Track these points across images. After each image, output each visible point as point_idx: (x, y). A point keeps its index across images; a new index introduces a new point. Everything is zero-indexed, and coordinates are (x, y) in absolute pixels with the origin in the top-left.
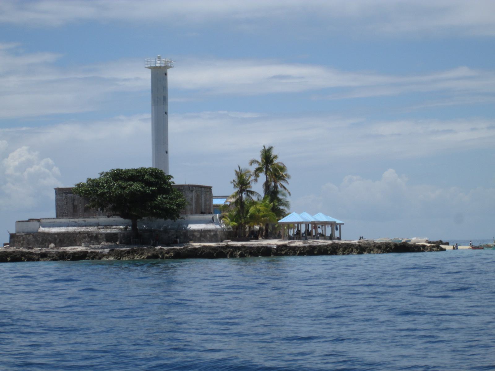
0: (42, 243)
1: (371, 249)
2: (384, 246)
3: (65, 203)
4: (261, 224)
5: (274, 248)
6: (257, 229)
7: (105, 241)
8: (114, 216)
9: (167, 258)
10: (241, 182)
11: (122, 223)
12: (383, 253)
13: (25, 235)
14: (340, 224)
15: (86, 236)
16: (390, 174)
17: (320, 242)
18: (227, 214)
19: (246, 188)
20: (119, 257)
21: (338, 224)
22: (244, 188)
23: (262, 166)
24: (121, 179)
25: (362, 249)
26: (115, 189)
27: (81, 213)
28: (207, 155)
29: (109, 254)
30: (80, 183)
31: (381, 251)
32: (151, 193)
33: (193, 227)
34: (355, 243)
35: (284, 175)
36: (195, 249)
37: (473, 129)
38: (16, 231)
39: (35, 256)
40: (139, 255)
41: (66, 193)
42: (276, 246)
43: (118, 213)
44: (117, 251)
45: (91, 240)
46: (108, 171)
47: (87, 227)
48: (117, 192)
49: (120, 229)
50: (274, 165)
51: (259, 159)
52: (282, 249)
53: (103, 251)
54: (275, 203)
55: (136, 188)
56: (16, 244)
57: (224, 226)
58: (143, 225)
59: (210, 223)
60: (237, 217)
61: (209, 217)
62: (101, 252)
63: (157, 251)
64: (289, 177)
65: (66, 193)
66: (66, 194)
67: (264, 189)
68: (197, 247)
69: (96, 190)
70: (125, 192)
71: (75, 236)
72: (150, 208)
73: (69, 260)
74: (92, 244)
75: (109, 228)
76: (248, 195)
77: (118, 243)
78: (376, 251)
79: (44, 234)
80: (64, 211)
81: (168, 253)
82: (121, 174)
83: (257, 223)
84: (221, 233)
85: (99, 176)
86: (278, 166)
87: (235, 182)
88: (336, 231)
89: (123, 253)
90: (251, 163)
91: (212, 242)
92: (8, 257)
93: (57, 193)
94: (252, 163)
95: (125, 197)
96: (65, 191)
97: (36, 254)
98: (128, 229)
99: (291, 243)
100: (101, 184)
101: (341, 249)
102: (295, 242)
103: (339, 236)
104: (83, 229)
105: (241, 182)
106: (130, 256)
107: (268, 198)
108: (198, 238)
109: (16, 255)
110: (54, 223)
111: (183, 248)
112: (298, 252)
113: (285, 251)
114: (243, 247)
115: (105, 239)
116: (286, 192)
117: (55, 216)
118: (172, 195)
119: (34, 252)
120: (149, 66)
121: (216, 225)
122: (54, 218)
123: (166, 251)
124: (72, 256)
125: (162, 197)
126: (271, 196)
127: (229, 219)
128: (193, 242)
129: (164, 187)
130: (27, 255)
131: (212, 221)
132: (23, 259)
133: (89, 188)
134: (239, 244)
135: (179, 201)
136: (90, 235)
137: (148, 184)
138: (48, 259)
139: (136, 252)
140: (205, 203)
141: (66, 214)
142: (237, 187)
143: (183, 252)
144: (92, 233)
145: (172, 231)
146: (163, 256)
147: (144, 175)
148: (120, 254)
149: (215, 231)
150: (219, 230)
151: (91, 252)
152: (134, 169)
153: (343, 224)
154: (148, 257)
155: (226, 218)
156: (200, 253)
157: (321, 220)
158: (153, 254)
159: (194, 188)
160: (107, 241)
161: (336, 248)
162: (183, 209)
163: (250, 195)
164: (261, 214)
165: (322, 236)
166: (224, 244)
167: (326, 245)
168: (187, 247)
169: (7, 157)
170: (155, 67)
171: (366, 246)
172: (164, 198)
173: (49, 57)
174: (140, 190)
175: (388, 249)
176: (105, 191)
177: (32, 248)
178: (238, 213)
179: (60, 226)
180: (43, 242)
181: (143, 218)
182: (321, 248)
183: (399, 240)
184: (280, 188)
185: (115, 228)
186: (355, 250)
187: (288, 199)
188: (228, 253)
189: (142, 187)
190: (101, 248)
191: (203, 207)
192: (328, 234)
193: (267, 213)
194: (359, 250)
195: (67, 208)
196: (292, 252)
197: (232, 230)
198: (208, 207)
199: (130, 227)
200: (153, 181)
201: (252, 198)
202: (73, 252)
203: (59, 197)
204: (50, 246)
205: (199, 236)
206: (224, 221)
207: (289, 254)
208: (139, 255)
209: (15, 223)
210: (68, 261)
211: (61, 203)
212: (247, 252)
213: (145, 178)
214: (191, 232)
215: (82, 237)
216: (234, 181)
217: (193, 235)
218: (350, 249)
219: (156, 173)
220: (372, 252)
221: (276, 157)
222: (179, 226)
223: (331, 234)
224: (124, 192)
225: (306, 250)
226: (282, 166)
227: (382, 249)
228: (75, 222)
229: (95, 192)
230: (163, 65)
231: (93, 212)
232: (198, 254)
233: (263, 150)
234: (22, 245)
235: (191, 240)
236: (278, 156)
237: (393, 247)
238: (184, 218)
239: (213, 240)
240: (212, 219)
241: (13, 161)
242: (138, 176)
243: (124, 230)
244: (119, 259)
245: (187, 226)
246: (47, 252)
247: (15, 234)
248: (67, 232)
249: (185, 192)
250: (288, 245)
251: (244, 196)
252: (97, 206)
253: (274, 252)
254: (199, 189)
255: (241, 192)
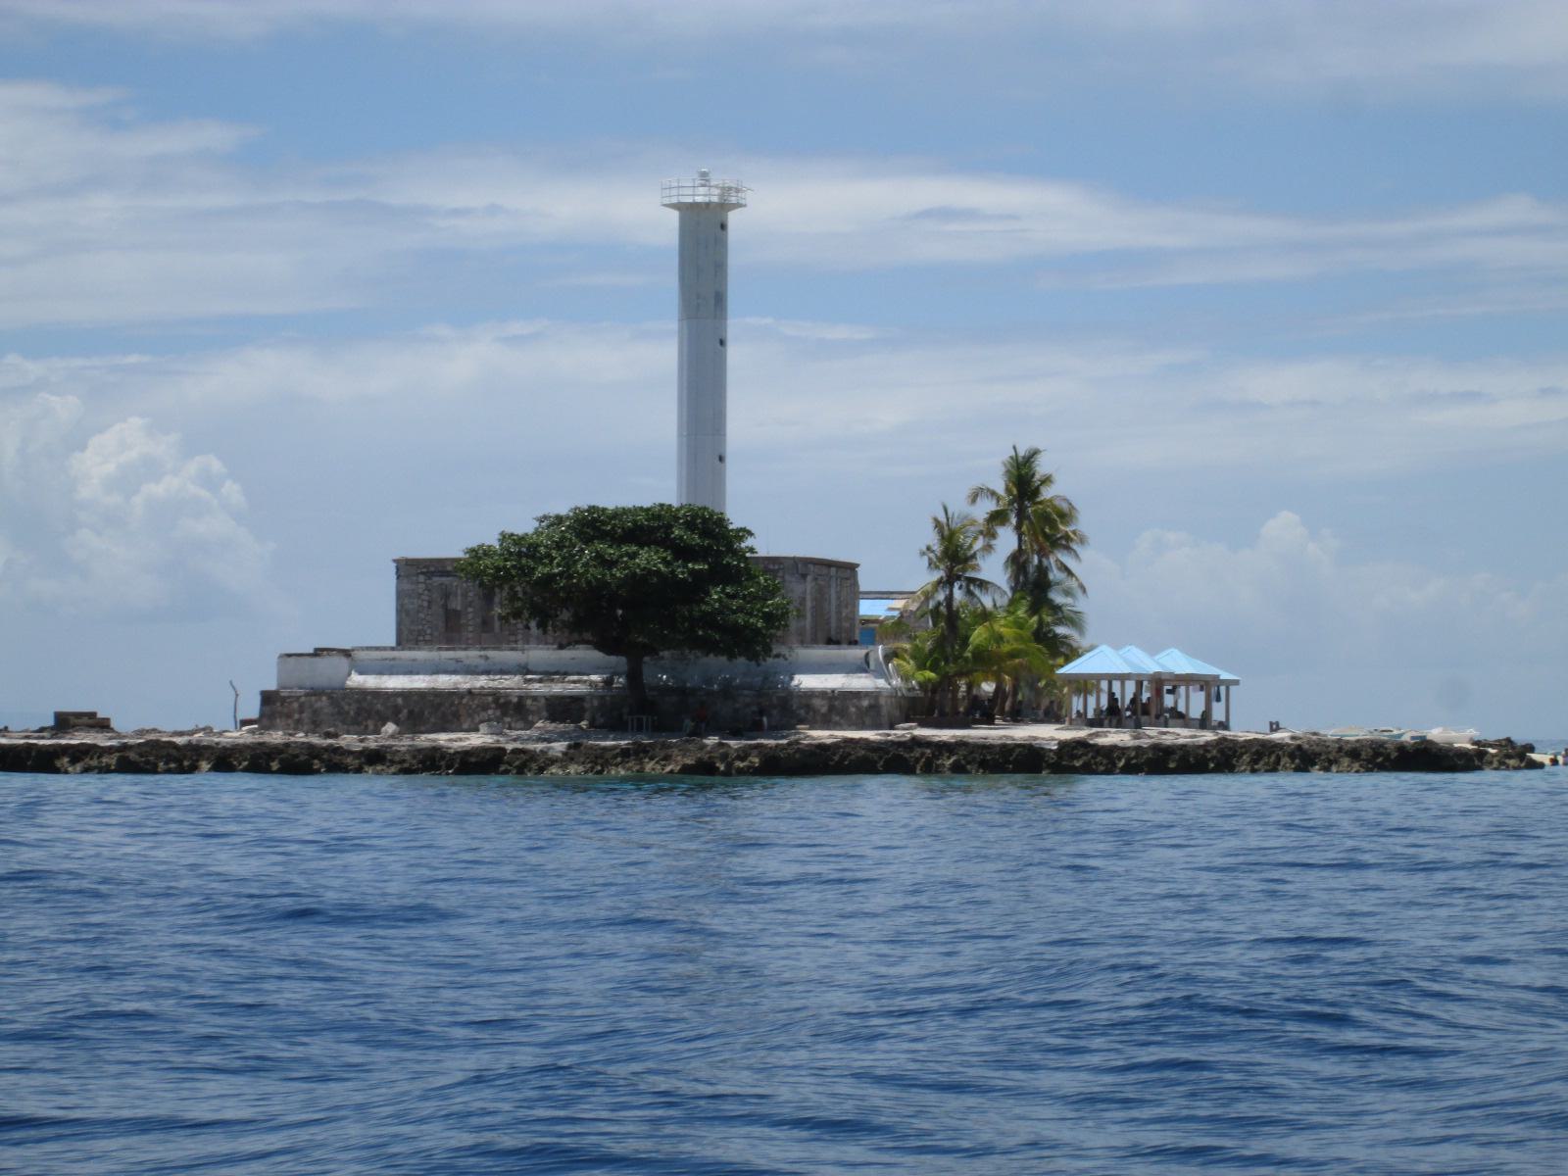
0: (356, 722)
1: (1332, 758)
2: (1369, 750)
3: (425, 604)
4: (1007, 677)
5: (1051, 750)
6: (989, 693)
7: (546, 719)
8: (577, 646)
9: (741, 772)
10: (950, 553)
11: (599, 668)
12: (1369, 770)
13: (307, 695)
14: (1229, 683)
15: (488, 703)
16: (1283, 527)
17: (1179, 735)
18: (907, 646)
19: (964, 570)
20: (599, 768)
21: (1224, 682)
22: (958, 570)
23: (1006, 507)
24: (603, 536)
25: (1307, 757)
26: (584, 565)
27: (470, 635)
28: (844, 469)
29: (568, 758)
30: (481, 546)
31: (1361, 766)
32: (690, 580)
33: (807, 682)
34: (1283, 739)
35: (1070, 534)
36: (822, 747)
37: (1546, 392)
38: (278, 684)
39: (349, 760)
40: (657, 763)
41: (429, 575)
42: (1056, 742)
43: (588, 636)
44: (592, 747)
45: (505, 714)
46: (563, 510)
47: (492, 677)
48: (592, 575)
49: (592, 684)
50: (1041, 503)
51: (1000, 487)
52: (1075, 752)
53: (549, 748)
54: (1044, 616)
55: (648, 563)
56: (278, 720)
57: (896, 682)
58: (660, 675)
59: (861, 672)
60: (936, 655)
61: (857, 653)
62: (541, 751)
63: (710, 752)
64: (1082, 541)
65: (429, 575)
66: (430, 578)
67: (1008, 575)
68: (829, 741)
69: (529, 567)
70: (614, 575)
71: (456, 702)
72: (686, 625)
73: (450, 772)
74: (507, 726)
75: (558, 681)
76: (969, 593)
77: (584, 724)
78: (1346, 764)
79: (363, 693)
80: (420, 627)
81: (742, 759)
82: (604, 523)
83: (990, 671)
84: (889, 701)
85: (537, 524)
86: (1054, 507)
87: (933, 551)
88: (1215, 705)
89: (608, 755)
90: (974, 498)
91: (861, 726)
92: (273, 761)
93: (402, 574)
94: (977, 495)
95: (615, 589)
96: (424, 567)
97: (351, 753)
98: (614, 686)
99: (1097, 735)
100: (542, 550)
101: (1244, 757)
102: (1109, 732)
103: (1224, 720)
104: (481, 682)
105: (950, 553)
106: (630, 764)
107: (1024, 601)
108: (824, 715)
109: (297, 756)
110: (392, 662)
111: (789, 744)
112: (1121, 764)
113: (1085, 758)
114: (961, 744)
115: (545, 714)
116: (1073, 583)
117: (392, 642)
118: (752, 587)
119: (345, 748)
120: (674, 200)
121: (876, 677)
122: (393, 649)
123: (737, 750)
124: (458, 760)
125: (723, 591)
126: (1031, 593)
127: (912, 662)
128: (807, 726)
129: (729, 564)
130: (325, 756)
131: (864, 667)
132: (315, 767)
133: (506, 560)
134: (946, 735)
135: (772, 604)
136: (502, 701)
137: (684, 552)
138: (388, 767)
139: (648, 752)
140: (839, 613)
141: (428, 638)
142: (937, 567)
143: (789, 754)
144: (507, 695)
145: (746, 692)
146: (729, 766)
147: (669, 527)
148: (602, 757)
149: (874, 695)
150: (885, 694)
151: (515, 751)
152: (641, 508)
153: (1236, 683)
154: (686, 770)
155: (905, 660)
156: (836, 758)
157: (1179, 671)
158: (700, 761)
159: (811, 567)
160: (553, 719)
161: (1230, 753)
162: (782, 628)
163: (977, 592)
164: (1006, 648)
165: (1180, 717)
166: (903, 736)
167: (1202, 743)
168: (797, 742)
169: (83, 447)
170: (691, 204)
171: (1317, 749)
172: (728, 595)
173: (216, 135)
174: (659, 569)
175: (1380, 760)
176: (556, 571)
177: (335, 736)
178: (940, 643)
179: (410, 670)
180: (360, 719)
181: (661, 654)
182: (1188, 751)
183: (1391, 734)
184: (1055, 575)
185: (574, 682)
186: (1285, 760)
187: (1081, 604)
188: (917, 760)
189: (664, 561)
190: (540, 740)
191: (834, 624)
192: (1196, 712)
193: (1022, 647)
194: (1297, 761)
195: (429, 618)
196: (1105, 762)
197: (920, 694)
198: (846, 625)
199: (621, 680)
200: (698, 544)
201: (980, 601)
202: (459, 750)
203: (407, 586)
204: (383, 729)
205: (824, 710)
206: (897, 668)
207: (1094, 767)
208: (657, 763)
209: (274, 660)
210: (448, 774)
211: (413, 604)
212: (974, 759)
213: (673, 536)
214: (800, 696)
215: (478, 706)
216: (928, 548)
217: (808, 707)
218: (1273, 758)
219: (705, 521)
220: (1334, 768)
221: (1047, 480)
222: (766, 678)
223: (1203, 712)
224: (612, 575)
225: (1145, 757)
226: (1064, 506)
227: (1364, 760)
228: (458, 661)
229: (525, 572)
230: (715, 199)
231: (507, 633)
232: (831, 763)
233: (1011, 458)
234: (298, 725)
235: (801, 722)
236: (1056, 477)
237: (1394, 755)
238: (784, 656)
239: (868, 721)
240: (863, 661)
241: (97, 464)
242: (652, 530)
243: (603, 688)
244: (600, 772)
245: (792, 679)
246: (382, 746)
247: (276, 693)
248: (433, 688)
249: (783, 577)
250: (1091, 742)
251: (958, 595)
252: (526, 614)
253: (1051, 761)
254: (825, 570)
255: (948, 581)
